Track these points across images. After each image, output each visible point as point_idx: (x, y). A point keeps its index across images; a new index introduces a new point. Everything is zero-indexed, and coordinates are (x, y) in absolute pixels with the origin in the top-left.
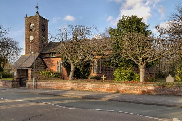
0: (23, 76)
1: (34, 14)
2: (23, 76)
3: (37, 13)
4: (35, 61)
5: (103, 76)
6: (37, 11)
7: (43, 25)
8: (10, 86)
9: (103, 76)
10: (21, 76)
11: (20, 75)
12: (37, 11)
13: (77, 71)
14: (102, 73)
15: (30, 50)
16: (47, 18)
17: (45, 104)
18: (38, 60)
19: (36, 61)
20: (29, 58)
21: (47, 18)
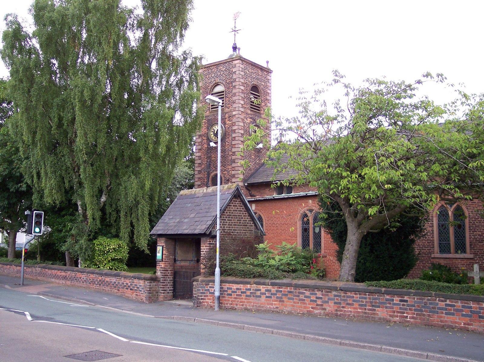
0: (183, 264)
1: (225, 54)
2: (183, 264)
3: (235, 48)
4: (222, 212)
5: (476, 267)
6: (235, 44)
7: (255, 88)
8: (144, 296)
9: (476, 267)
10: (178, 263)
11: (175, 260)
12: (235, 44)
13: (371, 242)
14: (472, 256)
15: (224, 122)
16: (268, 62)
17: (208, 359)
18: (233, 208)
19: (227, 213)
20: (177, 279)
21: (268, 62)
